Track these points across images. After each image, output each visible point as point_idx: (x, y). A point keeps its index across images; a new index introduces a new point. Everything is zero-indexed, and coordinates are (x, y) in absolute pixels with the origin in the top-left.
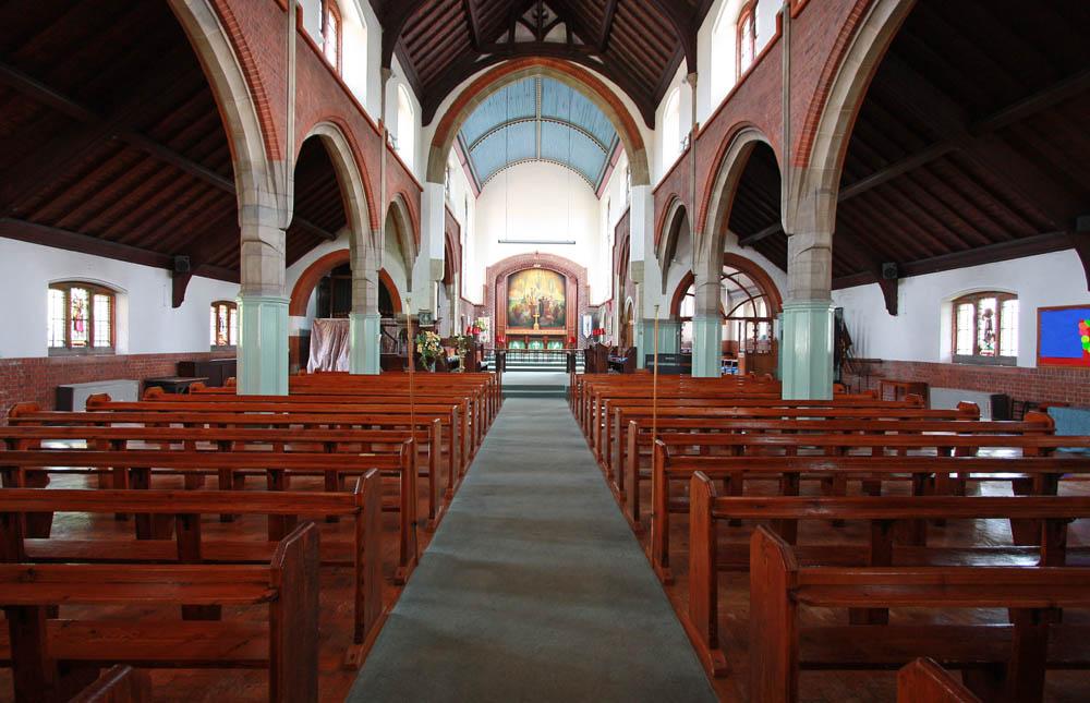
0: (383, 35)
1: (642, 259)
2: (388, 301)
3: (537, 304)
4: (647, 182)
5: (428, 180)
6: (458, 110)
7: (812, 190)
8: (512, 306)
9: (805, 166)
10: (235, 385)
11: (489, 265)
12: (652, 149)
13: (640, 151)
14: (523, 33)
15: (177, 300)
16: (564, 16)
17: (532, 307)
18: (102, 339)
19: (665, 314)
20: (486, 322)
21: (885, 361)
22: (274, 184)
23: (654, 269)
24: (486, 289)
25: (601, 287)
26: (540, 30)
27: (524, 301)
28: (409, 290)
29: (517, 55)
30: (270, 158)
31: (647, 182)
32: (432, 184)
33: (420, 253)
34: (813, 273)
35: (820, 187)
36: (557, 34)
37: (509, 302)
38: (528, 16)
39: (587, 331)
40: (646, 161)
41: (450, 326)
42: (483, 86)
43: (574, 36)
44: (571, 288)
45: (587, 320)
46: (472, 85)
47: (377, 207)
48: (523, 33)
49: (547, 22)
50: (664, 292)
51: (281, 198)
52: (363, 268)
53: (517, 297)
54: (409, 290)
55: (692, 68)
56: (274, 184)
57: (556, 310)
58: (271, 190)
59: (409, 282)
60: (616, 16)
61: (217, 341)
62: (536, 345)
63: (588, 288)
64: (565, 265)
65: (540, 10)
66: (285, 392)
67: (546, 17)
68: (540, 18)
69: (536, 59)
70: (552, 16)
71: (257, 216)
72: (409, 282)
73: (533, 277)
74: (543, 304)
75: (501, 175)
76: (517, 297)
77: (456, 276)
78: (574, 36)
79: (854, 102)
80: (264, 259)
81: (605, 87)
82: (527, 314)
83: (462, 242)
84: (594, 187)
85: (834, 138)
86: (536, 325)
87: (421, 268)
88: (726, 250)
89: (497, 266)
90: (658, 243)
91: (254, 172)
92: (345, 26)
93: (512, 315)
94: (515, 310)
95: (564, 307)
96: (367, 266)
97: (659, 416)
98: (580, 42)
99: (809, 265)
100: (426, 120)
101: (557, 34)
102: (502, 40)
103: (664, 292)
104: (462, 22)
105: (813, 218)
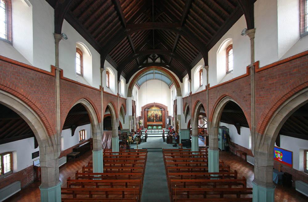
0: (118, 73)
1: (180, 114)
2: (120, 128)
3: (155, 115)
4: (181, 96)
5: (128, 97)
6: (135, 80)
7: (213, 127)
8: (148, 116)
9: (212, 122)
10: (92, 163)
11: (143, 106)
12: (182, 88)
13: (179, 88)
14: (150, 60)
15: (73, 134)
16: (160, 56)
17: (154, 116)
18: (83, 139)
19: (186, 128)
20: (142, 121)
21: (239, 145)
22: (100, 127)
23: (183, 117)
24: (142, 112)
25: (171, 113)
26: (154, 60)
27: (151, 115)
28: (124, 123)
29: (148, 66)
30: (99, 122)
31: (181, 96)
32: (166, 106)
33: (126, 114)
34: (214, 144)
35: (215, 127)
36: (158, 60)
37: (147, 115)
38: (151, 56)
39: (168, 123)
40: (180, 91)
41: (133, 126)
42: (140, 73)
43: (162, 60)
44: (163, 112)
45: (168, 120)
46: (139, 72)
47: (117, 112)
48: (150, 60)
49: (156, 57)
50: (186, 122)
51: (101, 130)
52: (115, 127)
53: (150, 114)
54: (124, 123)
55: (190, 78)
56: (100, 127)
57: (160, 117)
58: (99, 128)
59: (124, 121)
60: (179, 42)
61: (80, 140)
62: (155, 127)
63: (168, 111)
64: (161, 106)
65: (154, 55)
66: (103, 172)
67: (155, 56)
68: (154, 56)
69: (153, 67)
70: (157, 56)
71: (96, 135)
72: (124, 121)
73: (154, 108)
74: (156, 115)
75: (145, 83)
76: (150, 114)
77: (135, 114)
78: (162, 60)
79: (220, 113)
80: (98, 143)
81: (170, 73)
82: (152, 118)
83: (136, 105)
84: (169, 85)
85: (217, 118)
86: (155, 121)
87: (127, 118)
88: (200, 112)
89: (144, 106)
90: (184, 111)
91: (96, 126)
92: (110, 75)
93: (148, 118)
94: (149, 117)
95: (162, 116)
96: (116, 127)
97: (176, 189)
98: (164, 62)
99: (213, 142)
100: (127, 82)
101: (158, 60)
102: (145, 62)
103: (186, 122)
104: (129, 48)
105: (213, 133)
